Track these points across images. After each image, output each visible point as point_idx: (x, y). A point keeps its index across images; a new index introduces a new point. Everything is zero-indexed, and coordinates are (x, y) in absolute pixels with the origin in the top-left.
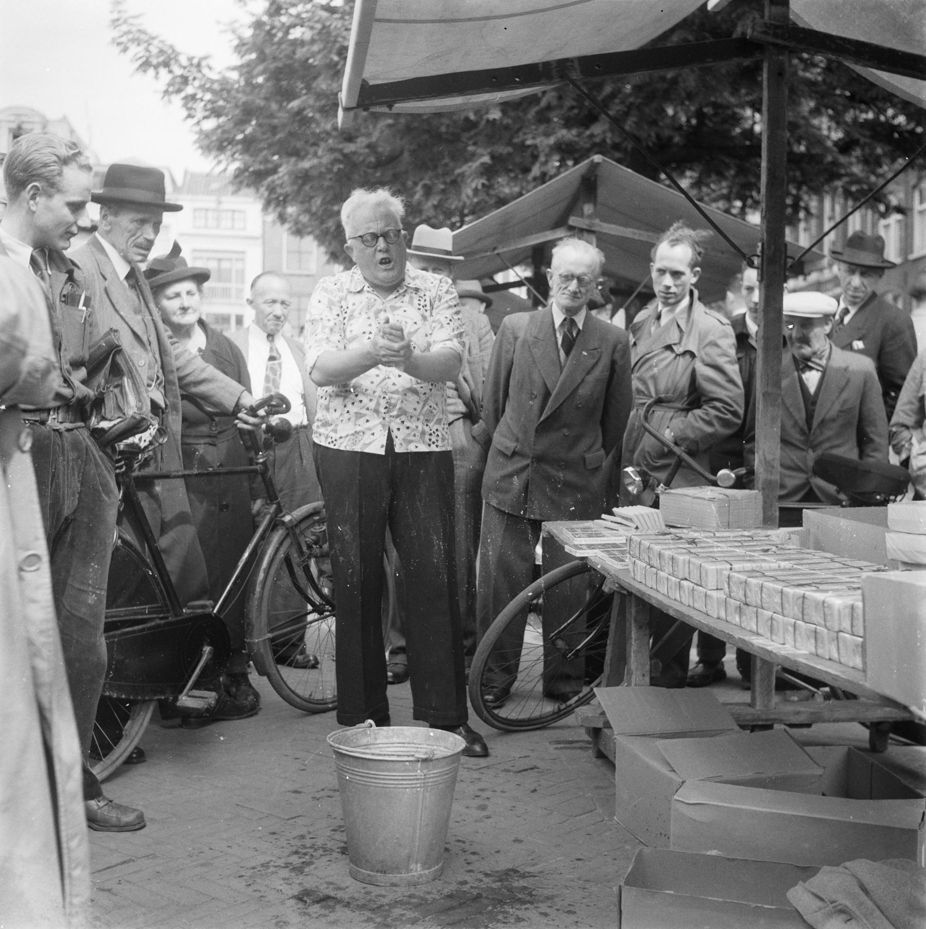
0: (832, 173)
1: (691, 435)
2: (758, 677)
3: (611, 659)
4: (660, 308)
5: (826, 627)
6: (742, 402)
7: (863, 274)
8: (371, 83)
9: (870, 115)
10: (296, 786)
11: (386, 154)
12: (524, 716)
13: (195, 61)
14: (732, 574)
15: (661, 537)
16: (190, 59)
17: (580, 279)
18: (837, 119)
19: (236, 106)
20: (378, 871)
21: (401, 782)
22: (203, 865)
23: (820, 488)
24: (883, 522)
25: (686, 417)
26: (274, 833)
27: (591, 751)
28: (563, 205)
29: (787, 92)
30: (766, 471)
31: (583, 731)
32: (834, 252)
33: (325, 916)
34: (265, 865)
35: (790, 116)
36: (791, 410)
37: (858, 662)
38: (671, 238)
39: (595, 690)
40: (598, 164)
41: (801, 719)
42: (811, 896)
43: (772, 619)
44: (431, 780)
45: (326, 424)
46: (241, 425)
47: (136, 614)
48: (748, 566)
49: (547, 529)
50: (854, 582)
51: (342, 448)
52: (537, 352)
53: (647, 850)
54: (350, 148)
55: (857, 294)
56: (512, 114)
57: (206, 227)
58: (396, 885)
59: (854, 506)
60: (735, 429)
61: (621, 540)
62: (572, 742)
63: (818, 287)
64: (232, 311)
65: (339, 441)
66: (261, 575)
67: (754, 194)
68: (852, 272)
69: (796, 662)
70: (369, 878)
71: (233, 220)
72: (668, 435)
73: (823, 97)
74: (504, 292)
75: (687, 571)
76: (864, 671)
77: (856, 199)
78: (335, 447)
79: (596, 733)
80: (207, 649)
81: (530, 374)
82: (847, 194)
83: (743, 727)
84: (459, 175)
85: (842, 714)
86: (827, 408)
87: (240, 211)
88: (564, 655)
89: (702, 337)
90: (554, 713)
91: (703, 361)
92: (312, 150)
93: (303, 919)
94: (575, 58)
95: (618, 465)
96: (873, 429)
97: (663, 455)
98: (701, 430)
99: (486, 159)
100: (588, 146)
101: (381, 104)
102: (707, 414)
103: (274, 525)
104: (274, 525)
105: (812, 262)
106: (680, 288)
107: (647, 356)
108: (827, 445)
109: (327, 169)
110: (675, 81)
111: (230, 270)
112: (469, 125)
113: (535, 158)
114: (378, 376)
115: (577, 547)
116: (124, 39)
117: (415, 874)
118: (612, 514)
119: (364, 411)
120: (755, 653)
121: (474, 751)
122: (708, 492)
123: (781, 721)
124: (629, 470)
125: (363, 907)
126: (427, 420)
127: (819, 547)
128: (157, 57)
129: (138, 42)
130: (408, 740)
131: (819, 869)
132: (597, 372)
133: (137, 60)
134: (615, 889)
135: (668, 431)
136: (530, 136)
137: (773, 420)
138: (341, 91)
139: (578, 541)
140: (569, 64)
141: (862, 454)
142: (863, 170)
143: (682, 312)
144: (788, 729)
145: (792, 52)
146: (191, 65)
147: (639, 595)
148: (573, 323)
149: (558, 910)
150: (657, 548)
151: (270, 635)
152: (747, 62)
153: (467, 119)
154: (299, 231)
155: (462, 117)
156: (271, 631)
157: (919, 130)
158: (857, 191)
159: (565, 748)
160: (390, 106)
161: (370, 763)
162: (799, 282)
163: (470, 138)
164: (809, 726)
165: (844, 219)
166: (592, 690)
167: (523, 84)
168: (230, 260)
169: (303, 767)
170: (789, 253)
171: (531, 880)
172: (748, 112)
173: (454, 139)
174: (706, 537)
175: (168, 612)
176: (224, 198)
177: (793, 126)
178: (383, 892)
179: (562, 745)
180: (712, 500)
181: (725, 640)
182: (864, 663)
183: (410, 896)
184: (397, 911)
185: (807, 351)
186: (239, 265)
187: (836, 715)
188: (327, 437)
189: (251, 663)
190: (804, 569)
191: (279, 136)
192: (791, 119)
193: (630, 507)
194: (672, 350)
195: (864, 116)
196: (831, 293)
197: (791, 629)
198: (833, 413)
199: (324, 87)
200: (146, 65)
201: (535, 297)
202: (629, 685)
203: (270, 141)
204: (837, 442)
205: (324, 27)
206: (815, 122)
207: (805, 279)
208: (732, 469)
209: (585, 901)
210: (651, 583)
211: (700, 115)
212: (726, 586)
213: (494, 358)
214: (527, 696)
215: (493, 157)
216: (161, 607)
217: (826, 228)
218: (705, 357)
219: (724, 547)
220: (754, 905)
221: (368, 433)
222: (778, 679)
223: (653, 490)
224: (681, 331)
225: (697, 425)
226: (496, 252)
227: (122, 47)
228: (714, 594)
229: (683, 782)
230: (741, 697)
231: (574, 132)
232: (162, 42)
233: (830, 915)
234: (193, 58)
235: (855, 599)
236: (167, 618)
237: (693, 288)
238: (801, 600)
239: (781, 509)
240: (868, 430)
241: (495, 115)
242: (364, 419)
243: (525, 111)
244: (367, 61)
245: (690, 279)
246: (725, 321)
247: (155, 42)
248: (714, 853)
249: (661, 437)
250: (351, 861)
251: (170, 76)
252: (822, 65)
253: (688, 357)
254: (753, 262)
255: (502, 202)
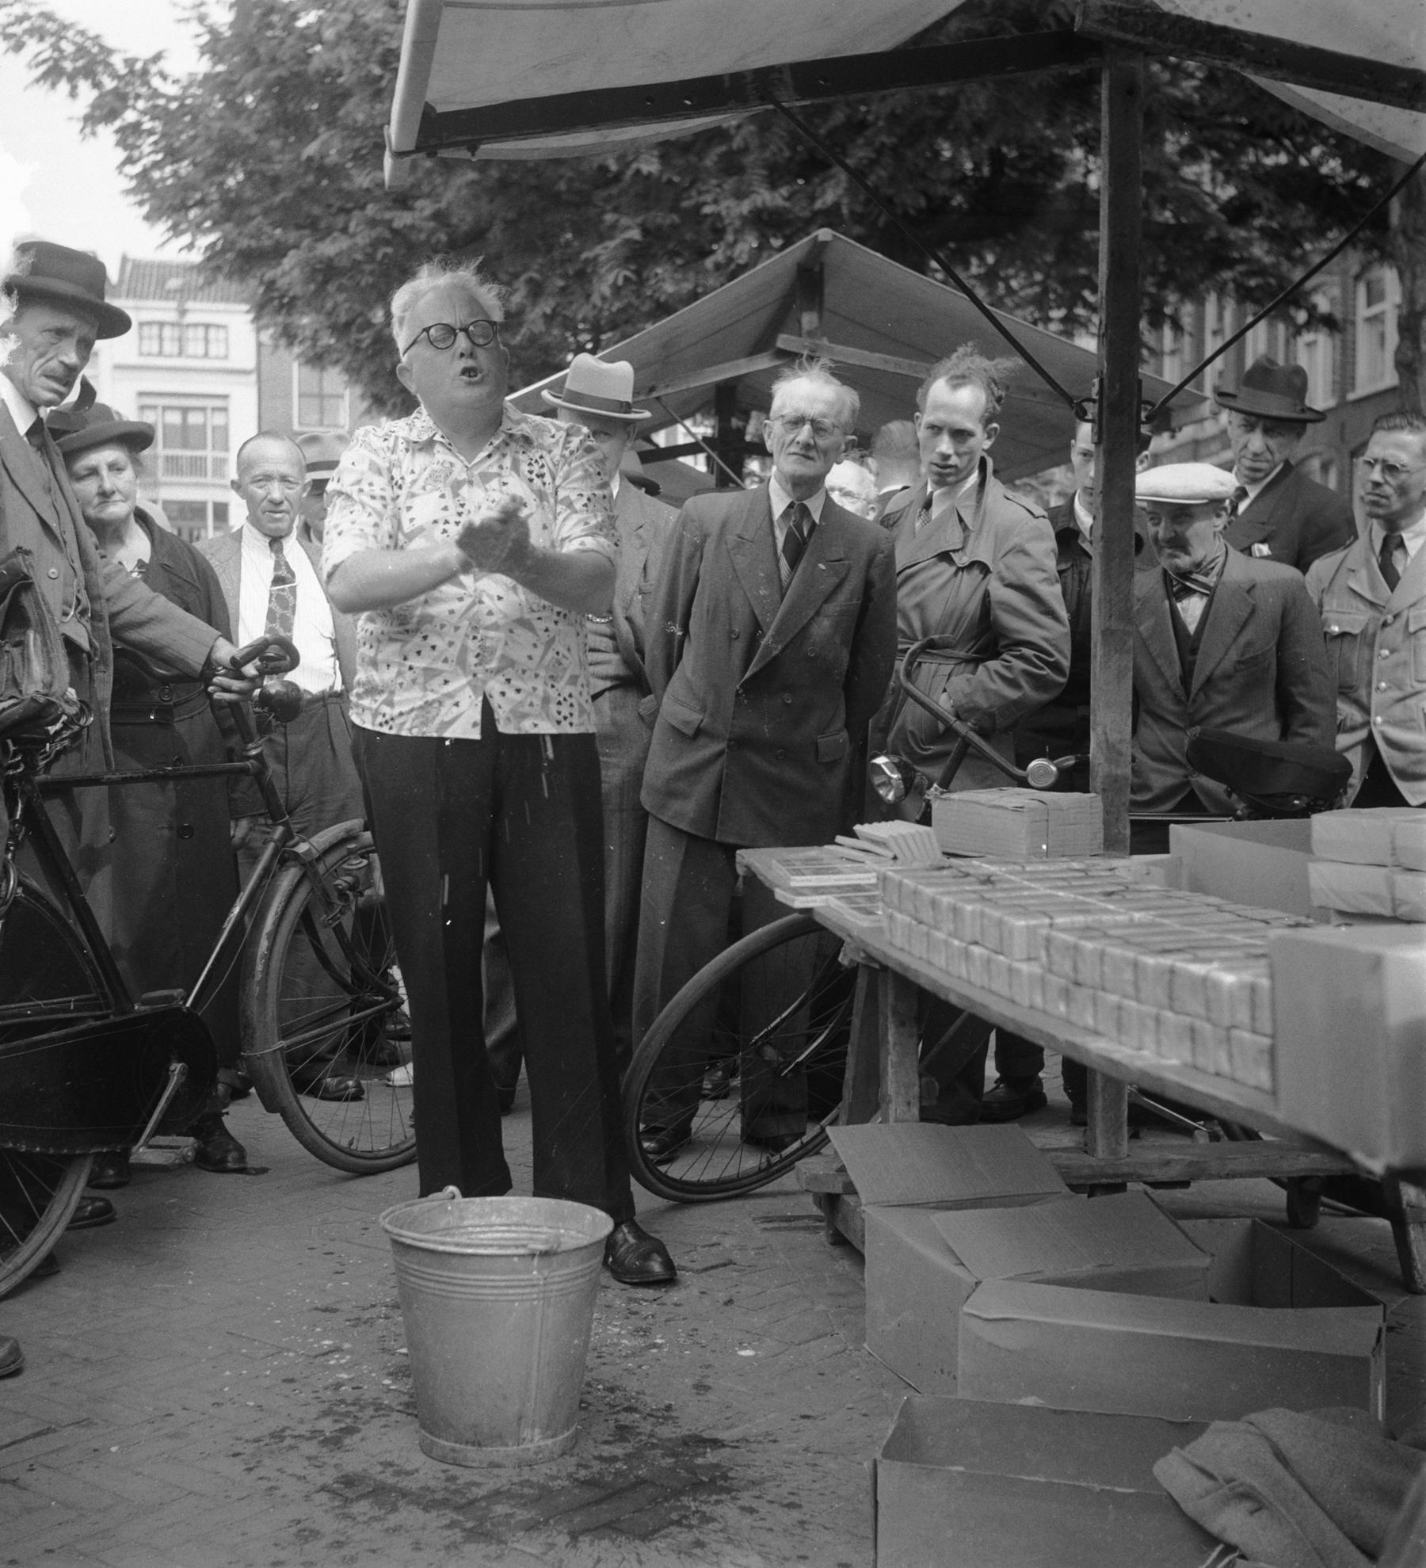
0: (1218, 257)
1: (982, 702)
2: (1098, 1104)
3: (854, 1079)
4: (929, 489)
5: (1209, 1020)
6: (1067, 648)
7: (1267, 431)
8: (440, 109)
9: (1283, 159)
10: (328, 1301)
11: (464, 227)
12: (711, 1175)
13: (138, 66)
14: (1054, 933)
15: (936, 873)
16: (130, 62)
17: (817, 427)
18: (1226, 167)
19: (209, 141)
20: (467, 1443)
21: (505, 1291)
22: (172, 1436)
23: (1202, 788)
24: (1304, 844)
25: (974, 672)
26: (292, 1381)
27: (822, 1233)
28: (763, 317)
29: (1141, 120)
30: (1109, 760)
31: (809, 1199)
32: (1221, 394)
33: (376, 1519)
34: (278, 1435)
35: (1146, 162)
36: (1160, 662)
37: (1263, 1077)
38: (952, 372)
39: (828, 1130)
40: (825, 244)
41: (1172, 1173)
42: (1192, 1471)
43: (1120, 1008)
44: (555, 1287)
45: (372, 690)
46: (218, 695)
47: (53, 1011)
48: (1080, 919)
49: (745, 861)
50: (1254, 946)
51: (404, 733)
52: (741, 561)
53: (917, 1399)
54: (402, 219)
55: (1258, 465)
56: (680, 162)
57: (160, 353)
58: (498, 1466)
59: (1256, 819)
60: (1056, 693)
61: (869, 879)
62: (788, 1219)
63: (1195, 452)
64: (209, 496)
65: (398, 721)
66: (264, 944)
67: (1087, 294)
68: (1250, 427)
69: (1160, 1079)
70: (452, 1454)
71: (207, 340)
72: (944, 703)
73: (1200, 129)
74: (670, 462)
75: (978, 929)
76: (1274, 1093)
77: (1257, 302)
78: (393, 732)
79: (831, 1203)
80: (177, 1067)
81: (728, 600)
82: (1245, 295)
83: (1075, 1188)
84: (587, 261)
85: (1241, 1163)
86: (1217, 657)
87: (218, 326)
88: (777, 1072)
89: (999, 538)
90: (760, 1171)
91: (1002, 579)
92: (340, 221)
93: (343, 1524)
94: (784, 65)
95: (862, 753)
96: (1301, 689)
97: (936, 737)
98: (997, 693)
99: (635, 234)
100: (807, 214)
101: (456, 145)
102: (1009, 668)
103: (284, 857)
104: (284, 857)
105: (1185, 407)
106: (966, 459)
107: (908, 571)
108: (1219, 720)
109: (366, 255)
110: (952, 103)
111: (204, 425)
112: (604, 178)
113: (718, 233)
114: (461, 599)
115: (798, 892)
116: (16, 29)
117: (529, 1446)
118: (853, 835)
119: (439, 665)
120: (1094, 1066)
121: (650, 1272)
122: (1013, 797)
123: (1139, 1178)
124: (881, 760)
125: (444, 1503)
126: (552, 677)
127: (1197, 886)
128: (75, 60)
129: (40, 33)
130: (515, 1219)
131: (1207, 1425)
132: (842, 598)
133: (38, 65)
134: (867, 1465)
135: (944, 696)
136: (708, 198)
137: (1120, 676)
138: (389, 123)
139: (797, 881)
140: (776, 75)
141: (1285, 732)
142: (1268, 253)
143: (967, 496)
144: (1149, 1189)
145: (1148, 53)
146: (132, 72)
147: (898, 969)
148: (805, 512)
149: (771, 1502)
150: (929, 891)
151: (283, 1043)
152: (1073, 71)
153: (603, 169)
154: (317, 359)
155: (595, 165)
156: (284, 1038)
157: (1364, 182)
158: (1257, 287)
159: (779, 1229)
160: (473, 149)
161: (454, 1261)
162: (1161, 442)
163: (608, 200)
164: (1185, 1184)
165: (1239, 336)
166: (823, 1130)
167: (699, 109)
168: (203, 409)
169: (340, 1268)
170: (1145, 396)
171: (726, 1452)
172: (1078, 153)
173: (582, 200)
174: (1011, 873)
175: (108, 1007)
176: (190, 305)
177: (1152, 180)
178: (477, 1479)
179: (776, 1225)
180: (1017, 809)
181: (1042, 1043)
182: (1274, 1078)
183: (522, 1484)
184: (500, 1509)
185: (1184, 561)
186: (218, 419)
187: (1231, 1166)
188: (375, 714)
189: (253, 1090)
190: (1172, 923)
191: (286, 194)
192: (1147, 168)
193: (883, 824)
194: (951, 562)
195: (1269, 161)
196: (1216, 459)
197: (1151, 1024)
198: (1227, 665)
199: (361, 117)
200: (53, 73)
201: (722, 471)
202: (885, 1121)
203: (267, 204)
204: (1239, 713)
205: (356, 17)
206: (1189, 171)
207: (1173, 437)
208: (1052, 758)
209: (816, 1486)
210: (919, 949)
211: (997, 159)
212: (1043, 953)
213: (667, 568)
214: (715, 1144)
215: (645, 231)
216: (96, 999)
217: (1208, 354)
218: (1006, 574)
219: (1041, 889)
220: (1097, 1487)
221: (449, 703)
222: (1131, 1106)
223: (922, 794)
224: (965, 528)
225: (993, 686)
226: (655, 394)
227: (12, 42)
228: (1024, 967)
229: (977, 1284)
230: (1061, 1138)
231: (784, 191)
232: (82, 33)
233: (1226, 1502)
234: (136, 60)
235: (1256, 975)
236: (107, 1016)
237: (985, 454)
238: (1167, 977)
239: (1133, 822)
240: (1294, 690)
241: (650, 166)
242: (439, 680)
243: (701, 155)
244: (432, 73)
245: (982, 443)
246: (1039, 511)
247: (70, 34)
248: (1030, 1401)
249: (934, 706)
250: (423, 1426)
251: (95, 93)
252: (1199, 74)
253: (976, 572)
254: (1085, 413)
255: (663, 309)
